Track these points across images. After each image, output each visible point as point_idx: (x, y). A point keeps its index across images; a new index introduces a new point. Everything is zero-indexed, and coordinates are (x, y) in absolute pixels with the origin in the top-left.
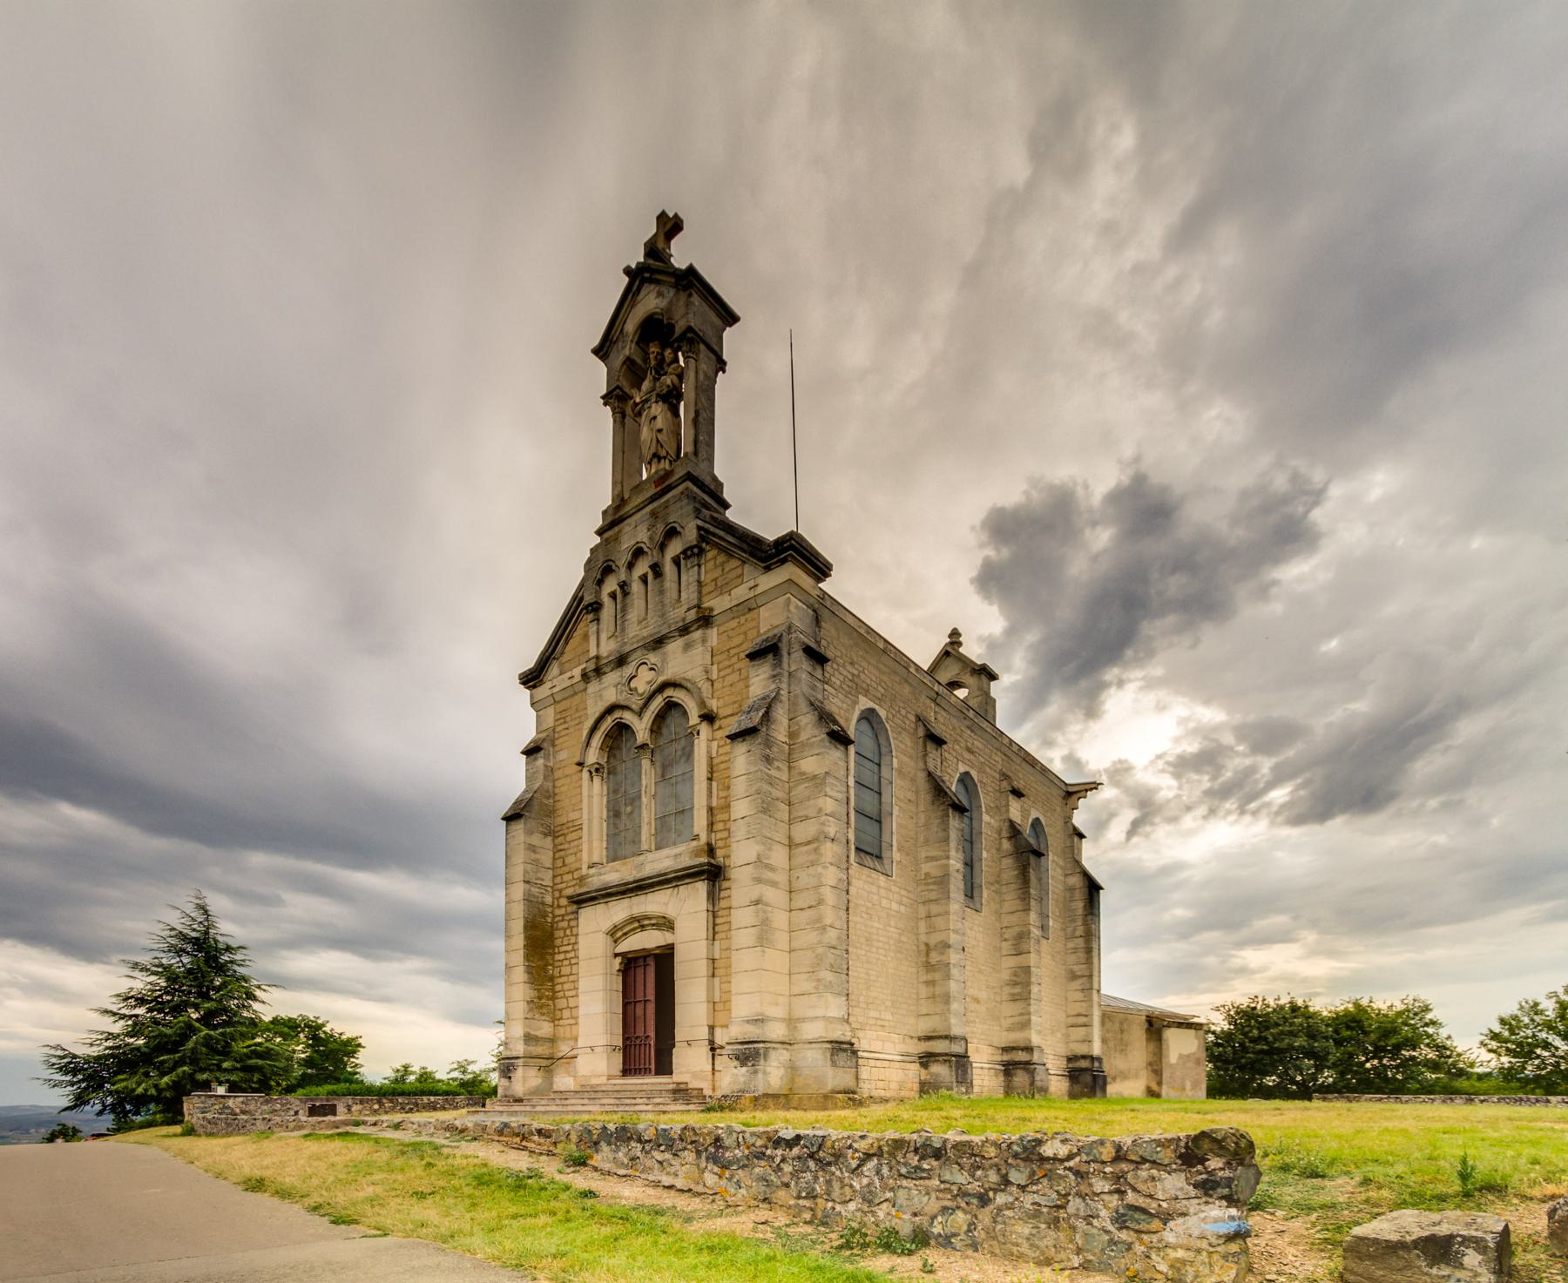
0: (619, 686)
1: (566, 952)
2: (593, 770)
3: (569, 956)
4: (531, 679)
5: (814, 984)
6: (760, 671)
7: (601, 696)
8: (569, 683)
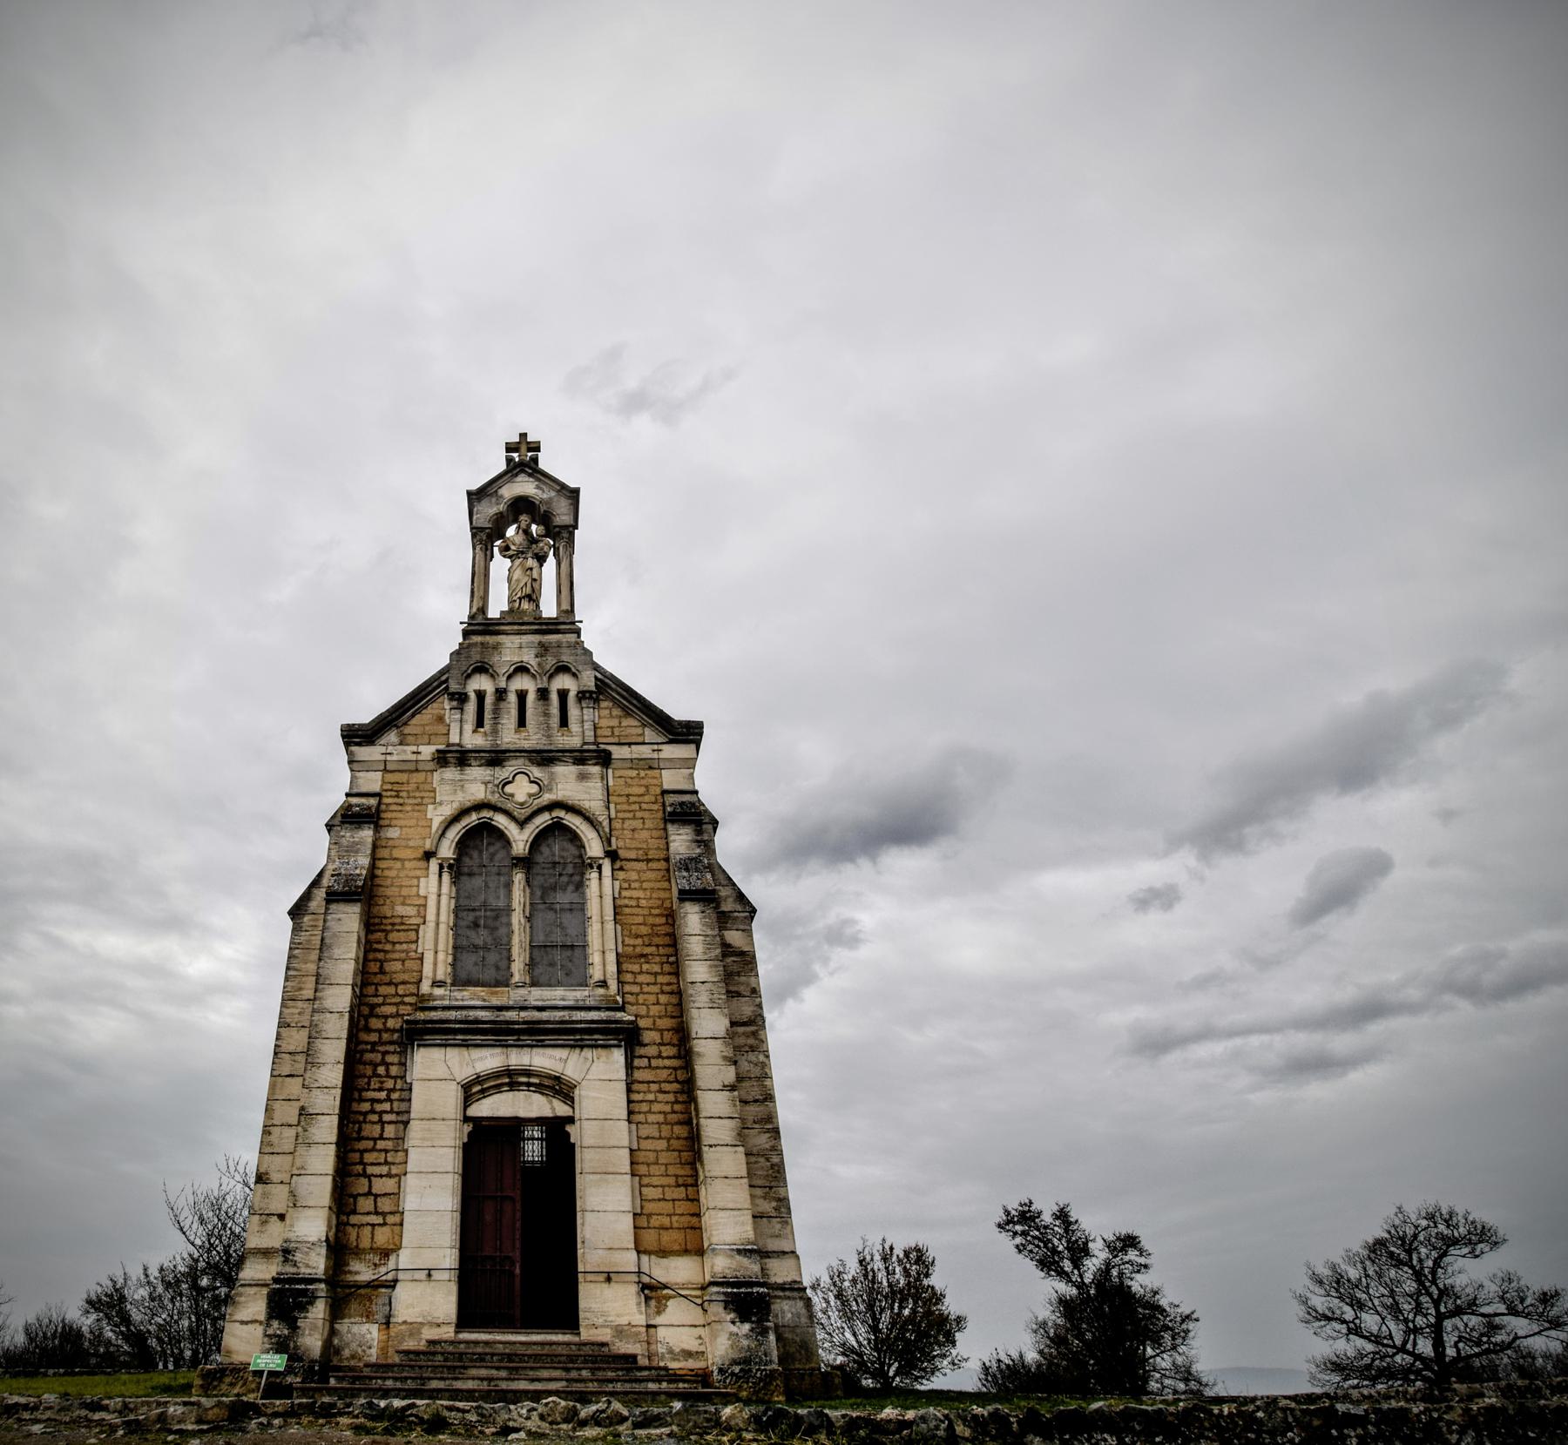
0: (490, 786)
1: (373, 1101)
2: (445, 865)
3: (378, 1107)
4: (354, 736)
5: (774, 1204)
6: (681, 831)
7: (462, 786)
8: (414, 757)
